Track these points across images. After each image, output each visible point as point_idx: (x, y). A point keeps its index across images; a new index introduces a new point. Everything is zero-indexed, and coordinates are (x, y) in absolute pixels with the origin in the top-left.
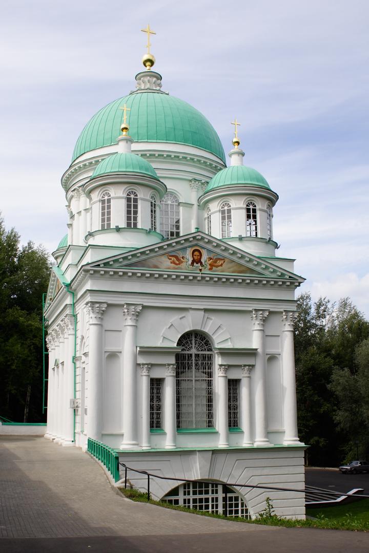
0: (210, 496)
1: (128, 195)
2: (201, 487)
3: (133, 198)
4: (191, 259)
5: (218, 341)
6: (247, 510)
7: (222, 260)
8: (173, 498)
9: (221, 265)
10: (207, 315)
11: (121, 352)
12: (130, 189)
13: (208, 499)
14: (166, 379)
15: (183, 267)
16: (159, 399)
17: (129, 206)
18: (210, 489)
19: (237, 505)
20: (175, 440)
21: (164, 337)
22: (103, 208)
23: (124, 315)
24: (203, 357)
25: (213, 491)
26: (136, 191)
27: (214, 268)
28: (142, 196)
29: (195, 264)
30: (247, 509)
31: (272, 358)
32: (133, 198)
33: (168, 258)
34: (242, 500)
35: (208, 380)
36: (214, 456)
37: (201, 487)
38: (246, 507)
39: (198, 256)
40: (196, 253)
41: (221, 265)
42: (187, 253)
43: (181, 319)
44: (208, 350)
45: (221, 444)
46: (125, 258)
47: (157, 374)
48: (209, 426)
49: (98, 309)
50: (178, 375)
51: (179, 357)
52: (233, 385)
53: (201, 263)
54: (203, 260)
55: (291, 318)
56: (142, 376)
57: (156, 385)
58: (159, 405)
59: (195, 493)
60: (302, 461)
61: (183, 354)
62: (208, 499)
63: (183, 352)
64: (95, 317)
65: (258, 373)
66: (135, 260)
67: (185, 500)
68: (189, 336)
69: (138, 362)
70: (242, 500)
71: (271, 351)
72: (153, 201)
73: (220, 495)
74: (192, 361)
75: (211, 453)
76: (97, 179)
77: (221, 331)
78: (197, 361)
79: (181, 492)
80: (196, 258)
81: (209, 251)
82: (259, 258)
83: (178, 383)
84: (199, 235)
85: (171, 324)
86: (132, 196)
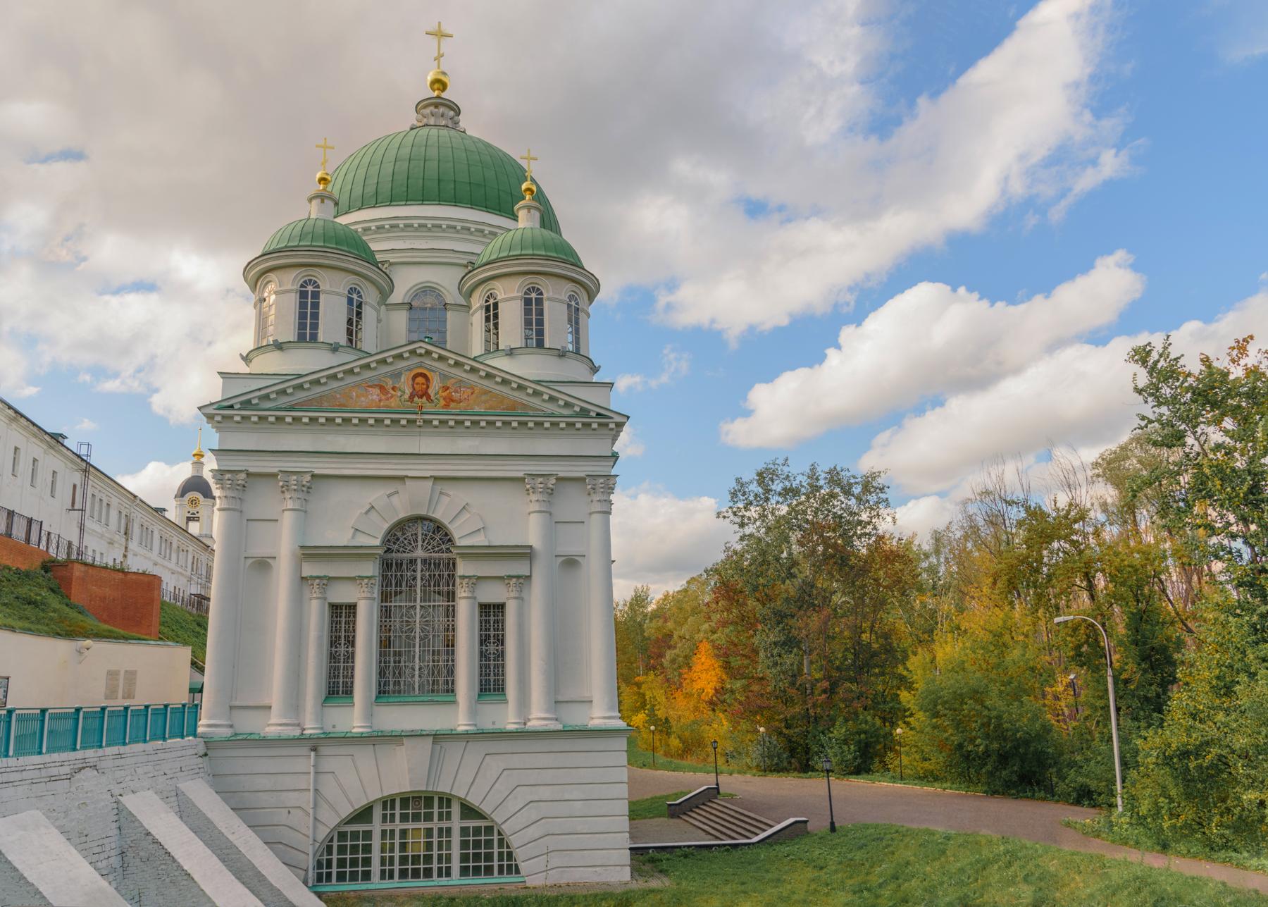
0: (435, 825)
3: (312, 291)
4: (408, 392)
5: (463, 534)
6: (510, 855)
8: (361, 828)
10: (439, 487)
11: (275, 558)
13: (431, 829)
17: (303, 305)
18: (436, 810)
19: (489, 844)
20: (473, 713)
22: (487, 319)
25: (441, 815)
26: (540, 287)
28: (551, 294)
29: (416, 399)
30: (511, 852)
31: (571, 563)
32: (312, 291)
34: (500, 834)
36: (438, 747)
38: (508, 847)
39: (423, 384)
40: (420, 380)
42: (402, 380)
43: (389, 496)
45: (459, 718)
46: (283, 392)
47: (343, 594)
48: (433, 691)
50: (385, 597)
51: (386, 565)
52: (491, 614)
53: (429, 398)
54: (431, 392)
55: (602, 488)
56: (311, 599)
57: (342, 615)
59: (404, 818)
60: (623, 758)
62: (431, 829)
64: (226, 497)
65: (537, 592)
66: (301, 395)
67: (384, 832)
69: (303, 575)
70: (500, 834)
71: (571, 550)
73: (456, 823)
75: (431, 738)
77: (466, 516)
79: (377, 813)
81: (444, 377)
82: (538, 382)
83: (386, 613)
84: (420, 347)
85: (368, 507)
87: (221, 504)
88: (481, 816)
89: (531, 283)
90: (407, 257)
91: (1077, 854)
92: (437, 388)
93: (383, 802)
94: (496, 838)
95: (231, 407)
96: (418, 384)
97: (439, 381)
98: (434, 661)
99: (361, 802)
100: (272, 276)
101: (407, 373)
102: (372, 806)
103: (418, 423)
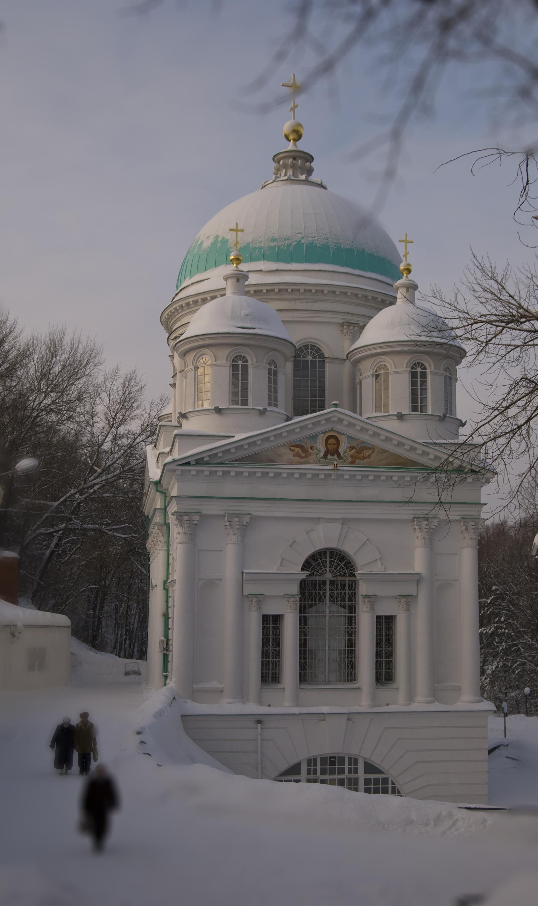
1: (412, 368)
2: (333, 763)
4: (323, 450)
7: (370, 449)
9: (369, 456)
12: (236, 353)
14: (285, 615)
15: (311, 461)
16: (389, 643)
21: (283, 559)
23: (226, 529)
24: (312, 584)
27: (358, 461)
29: (329, 456)
32: (420, 372)
33: (290, 449)
34: (393, 783)
35: (348, 616)
37: (333, 763)
39: (334, 444)
40: (331, 441)
41: (369, 456)
42: (318, 441)
44: (349, 576)
47: (271, 609)
49: (188, 522)
50: (302, 609)
53: (339, 455)
54: (341, 451)
58: (276, 650)
61: (312, 581)
63: (313, 578)
68: (333, 555)
70: (393, 783)
72: (448, 374)
74: (325, 590)
76: (369, 347)
78: (332, 590)
80: (330, 447)
81: (350, 438)
83: (303, 621)
84: (334, 416)
86: (419, 370)
87: (180, 539)
88: (380, 772)
89: (232, 356)
90: (293, 316)
91: (26, 376)
92: (345, 448)
93: (308, 760)
94: (390, 786)
95: (188, 463)
96: (330, 444)
97: (346, 442)
98: (348, 658)
99: (293, 761)
100: (206, 350)
101: (322, 435)
102: (300, 763)
103: (333, 477)
